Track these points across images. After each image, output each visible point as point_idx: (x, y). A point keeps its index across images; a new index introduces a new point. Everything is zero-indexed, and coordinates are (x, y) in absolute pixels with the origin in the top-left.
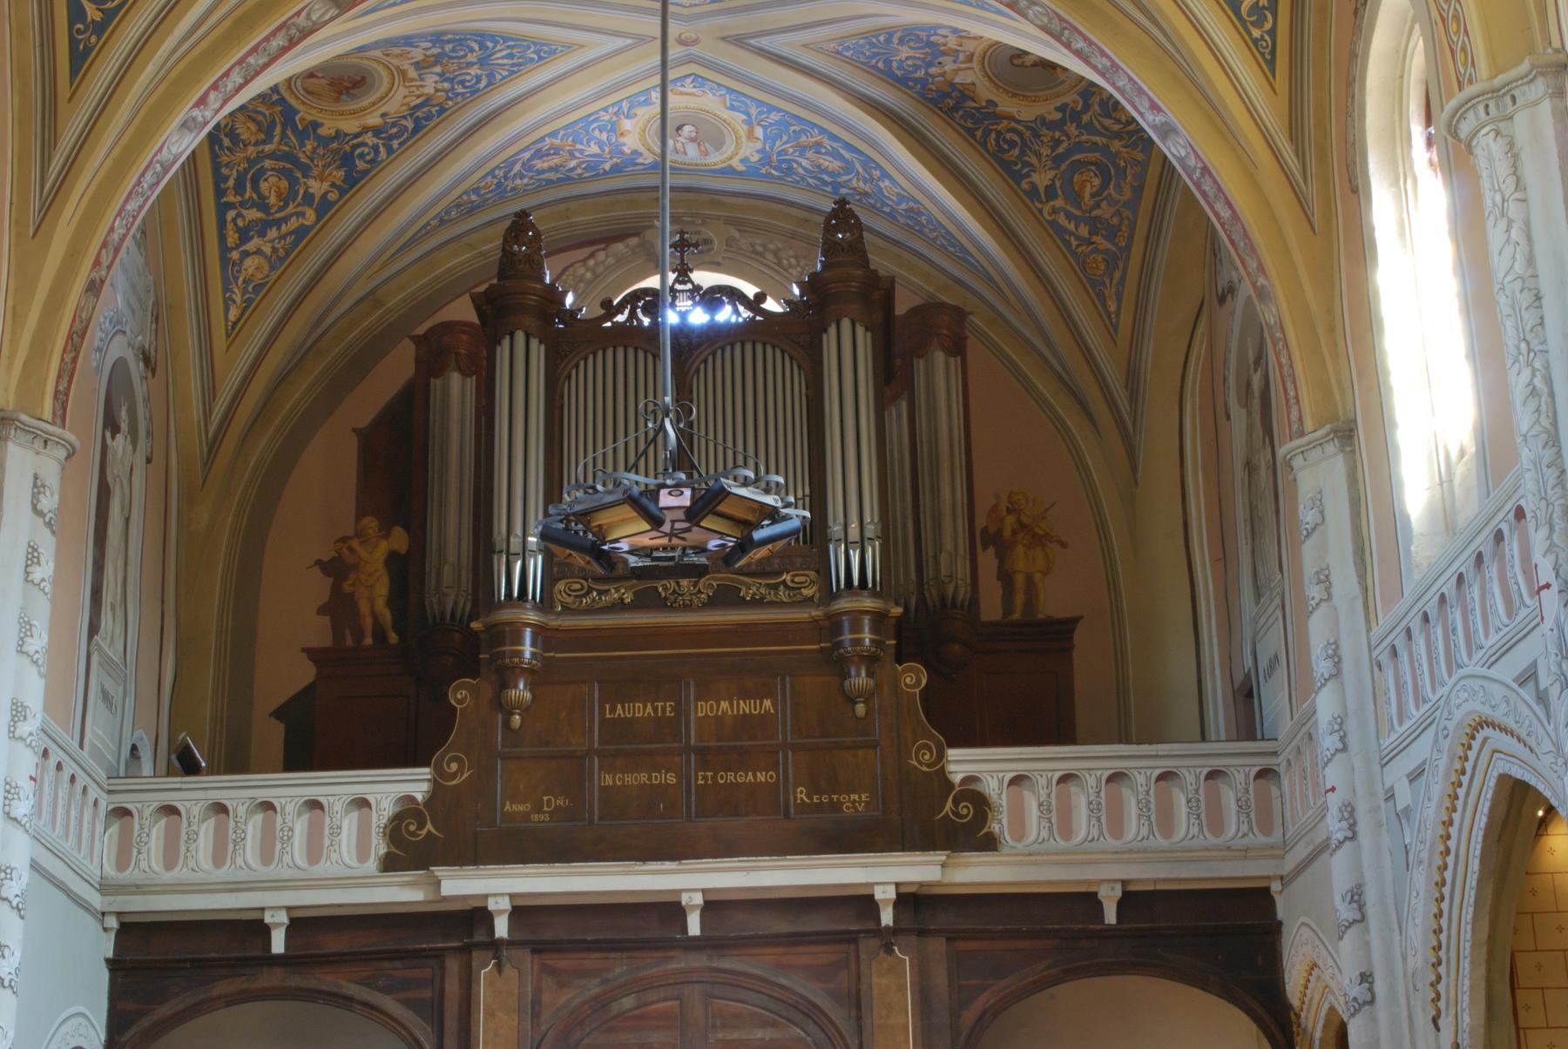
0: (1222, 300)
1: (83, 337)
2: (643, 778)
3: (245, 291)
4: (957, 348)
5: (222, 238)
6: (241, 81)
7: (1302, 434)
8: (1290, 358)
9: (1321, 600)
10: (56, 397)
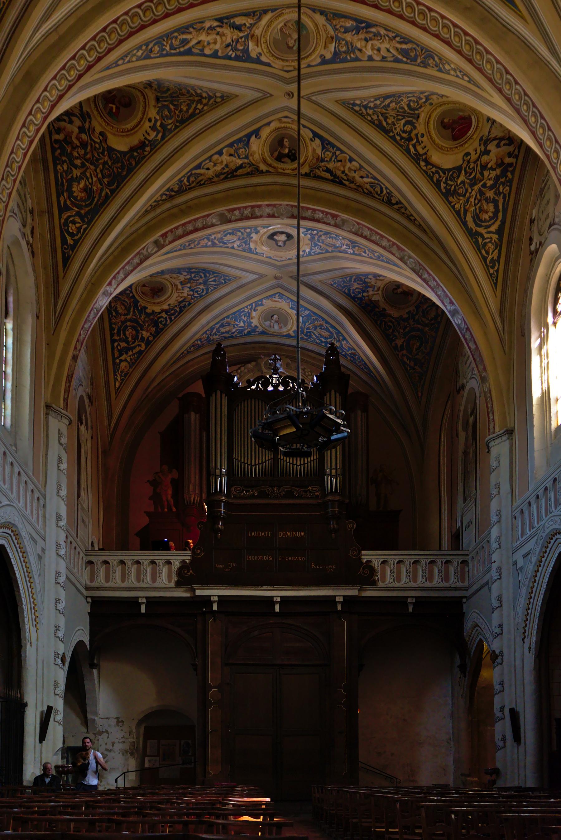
0: (458, 392)
1: (72, 378)
3: (121, 376)
6: (123, 276)
7: (494, 433)
8: (492, 404)
9: (496, 495)
10: (64, 400)
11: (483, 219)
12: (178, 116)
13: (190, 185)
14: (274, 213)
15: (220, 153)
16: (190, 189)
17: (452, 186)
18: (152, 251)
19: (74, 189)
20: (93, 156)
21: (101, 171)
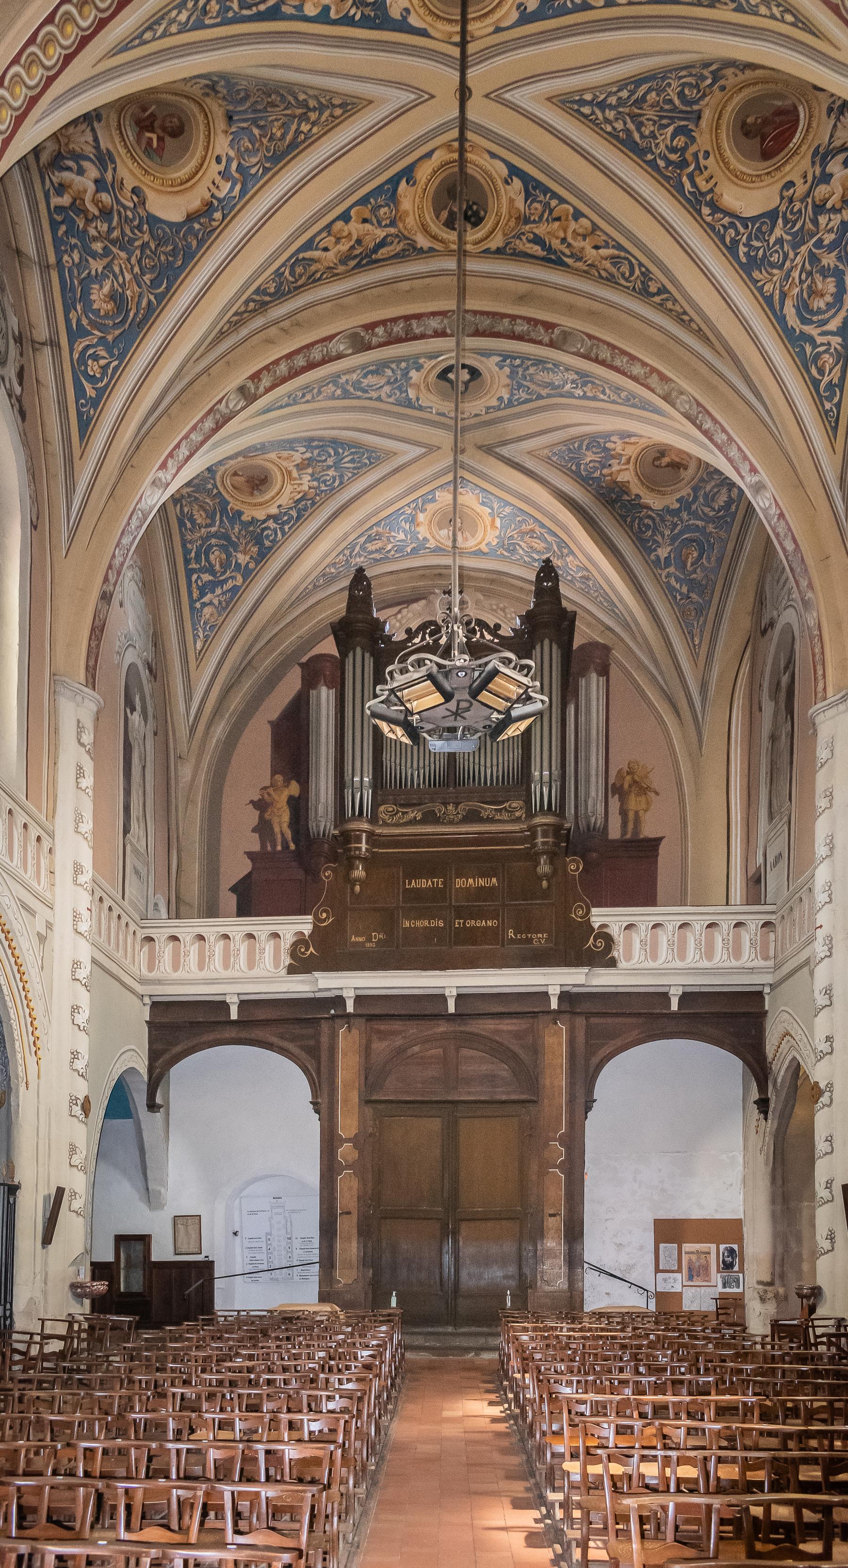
0: (764, 632)
2: (426, 923)
4: (604, 671)
5: (190, 593)
6: (187, 453)
7: (825, 699)
8: (822, 648)
11: (815, 309)
12: (268, 150)
13: (297, 281)
14: (445, 328)
15: (345, 217)
16: (296, 288)
17: (758, 249)
18: (235, 405)
19: (93, 297)
20: (123, 232)
21: (139, 262)
